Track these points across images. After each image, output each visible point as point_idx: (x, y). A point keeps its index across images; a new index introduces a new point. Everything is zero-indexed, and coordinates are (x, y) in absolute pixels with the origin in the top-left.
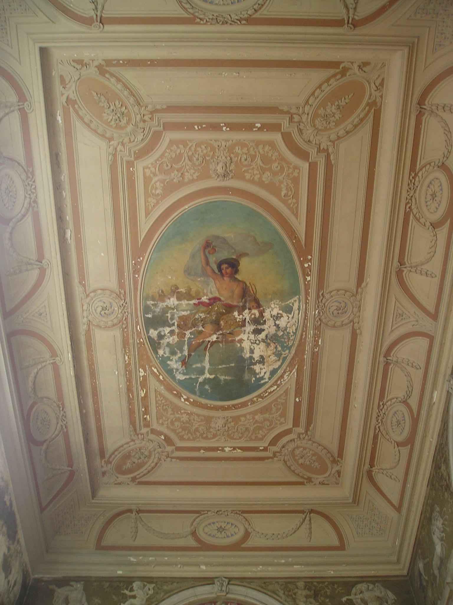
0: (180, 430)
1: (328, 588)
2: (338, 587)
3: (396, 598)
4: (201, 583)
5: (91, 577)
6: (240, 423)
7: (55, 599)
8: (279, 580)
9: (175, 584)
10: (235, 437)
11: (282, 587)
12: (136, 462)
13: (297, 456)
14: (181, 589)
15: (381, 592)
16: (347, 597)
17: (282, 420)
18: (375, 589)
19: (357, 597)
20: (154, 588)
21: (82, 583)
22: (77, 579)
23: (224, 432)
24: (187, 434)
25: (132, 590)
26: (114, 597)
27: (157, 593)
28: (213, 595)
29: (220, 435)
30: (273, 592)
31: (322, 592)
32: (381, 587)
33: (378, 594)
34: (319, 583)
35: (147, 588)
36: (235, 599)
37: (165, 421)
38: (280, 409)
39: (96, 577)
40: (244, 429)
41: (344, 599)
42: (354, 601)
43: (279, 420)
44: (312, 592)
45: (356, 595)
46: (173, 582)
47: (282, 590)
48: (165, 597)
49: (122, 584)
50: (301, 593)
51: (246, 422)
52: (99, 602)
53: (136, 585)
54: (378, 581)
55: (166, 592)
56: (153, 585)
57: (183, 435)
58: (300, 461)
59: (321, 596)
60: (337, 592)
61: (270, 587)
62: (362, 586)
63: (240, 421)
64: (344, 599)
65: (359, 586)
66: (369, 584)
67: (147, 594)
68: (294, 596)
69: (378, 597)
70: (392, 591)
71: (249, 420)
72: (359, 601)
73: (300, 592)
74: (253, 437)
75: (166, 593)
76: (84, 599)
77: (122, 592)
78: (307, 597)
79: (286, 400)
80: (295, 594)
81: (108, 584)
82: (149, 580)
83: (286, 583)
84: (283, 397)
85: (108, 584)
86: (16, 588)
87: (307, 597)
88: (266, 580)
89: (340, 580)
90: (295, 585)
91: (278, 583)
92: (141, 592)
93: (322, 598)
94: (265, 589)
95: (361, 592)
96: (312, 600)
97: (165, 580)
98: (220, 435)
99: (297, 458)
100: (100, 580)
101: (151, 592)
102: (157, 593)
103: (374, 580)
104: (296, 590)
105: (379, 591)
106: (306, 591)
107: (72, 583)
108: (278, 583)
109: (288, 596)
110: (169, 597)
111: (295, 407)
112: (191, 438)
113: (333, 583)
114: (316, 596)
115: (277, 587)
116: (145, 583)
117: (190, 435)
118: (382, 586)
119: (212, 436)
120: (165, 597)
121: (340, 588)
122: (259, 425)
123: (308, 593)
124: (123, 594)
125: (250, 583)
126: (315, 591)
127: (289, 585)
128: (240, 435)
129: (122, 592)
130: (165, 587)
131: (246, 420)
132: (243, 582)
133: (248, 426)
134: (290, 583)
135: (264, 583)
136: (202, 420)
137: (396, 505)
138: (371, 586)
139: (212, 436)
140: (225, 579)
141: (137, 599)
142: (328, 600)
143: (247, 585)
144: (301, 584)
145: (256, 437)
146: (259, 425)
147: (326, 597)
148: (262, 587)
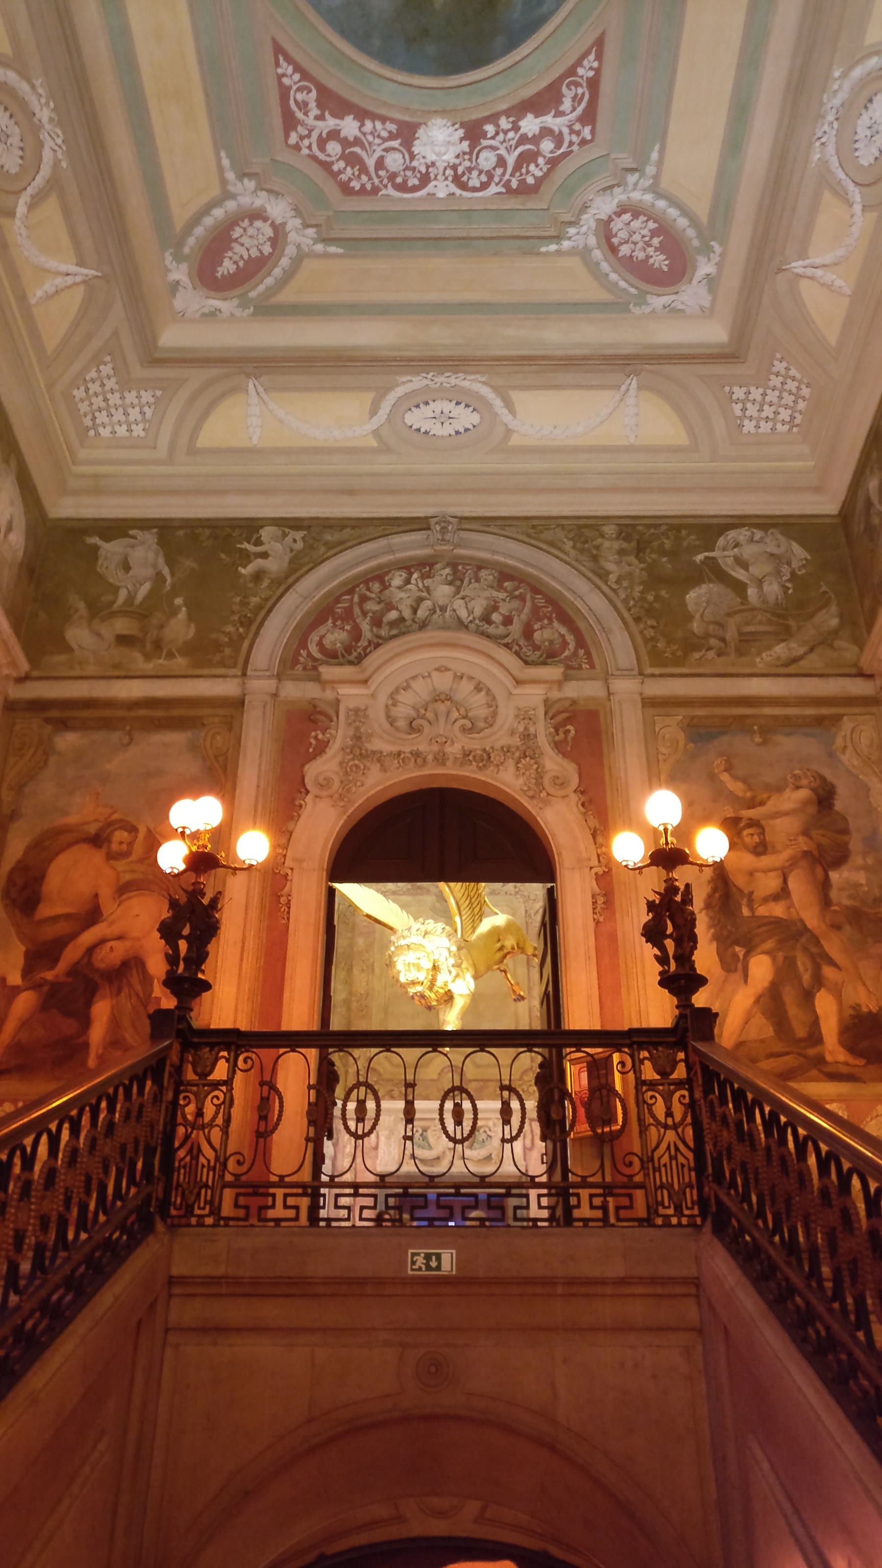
0: (342, 164)
1: (668, 538)
2: (689, 535)
3: (809, 557)
4: (400, 529)
5: (172, 520)
6: (485, 143)
7: (100, 562)
8: (565, 522)
9: (348, 529)
10: (471, 184)
11: (571, 535)
12: (246, 257)
13: (616, 235)
14: (360, 540)
15: (779, 547)
16: (706, 554)
17: (587, 132)
18: (767, 540)
19: (726, 553)
20: (303, 538)
21: (155, 530)
22: (145, 524)
23: (445, 169)
24: (359, 177)
25: (258, 542)
26: (223, 556)
27: (311, 547)
28: (428, 551)
29: (436, 179)
30: (552, 544)
31: (655, 544)
32: (780, 537)
33: (771, 548)
34: (650, 526)
35: (289, 539)
36: (471, 558)
37: (302, 138)
38: (583, 94)
39: (183, 520)
40: (493, 160)
41: (699, 558)
42: (720, 561)
43: (578, 133)
44: (634, 544)
45: (724, 549)
46: (343, 527)
47: (571, 539)
48: (329, 554)
49: (236, 533)
50: (610, 546)
51: (501, 137)
52: (194, 565)
53: (266, 533)
54: (774, 526)
55: (330, 546)
56: (302, 533)
57: (350, 180)
58: (625, 250)
59: (652, 551)
60: (685, 543)
61: (548, 535)
62: (741, 535)
63: (484, 135)
64: (699, 558)
65: (732, 534)
66: (755, 531)
67: (292, 551)
68: (595, 552)
69: (772, 555)
70: (802, 545)
71: (506, 132)
72: (730, 561)
73: (607, 544)
74: (514, 184)
75: (329, 549)
76: (161, 560)
77: (239, 546)
78: (621, 552)
79: (598, 71)
80: (597, 547)
81: (207, 532)
82: (295, 524)
83: (580, 527)
84: (591, 61)
85: (207, 532)
86: (12, 537)
87: (621, 552)
88: (535, 522)
89: (691, 521)
90: (598, 530)
91: (563, 527)
92: (278, 546)
93: (654, 556)
94: (537, 540)
95: (737, 545)
96: (632, 559)
97: (328, 524)
98: (436, 179)
99: (615, 241)
100: (192, 526)
101: (300, 545)
102: (311, 547)
103: (766, 523)
104: (600, 540)
105: (776, 543)
106: (621, 542)
107: (131, 532)
108: (563, 527)
109: (582, 551)
110: (335, 555)
111: (674, 71)
112: (369, 187)
113: (678, 528)
114: (639, 551)
115: (561, 534)
116: (287, 530)
117: (364, 178)
118: (782, 533)
119: (417, 182)
120: (329, 554)
121: (693, 537)
122: (528, 147)
123: (625, 545)
124: (241, 549)
125: (503, 527)
126: (638, 542)
127: (583, 530)
128: (484, 178)
129: (239, 546)
130: (328, 537)
131: (497, 133)
132: (489, 526)
133: (502, 151)
134: (586, 526)
135: (534, 527)
136: (392, 137)
137: (771, 822)
138: (758, 534)
139: (417, 182)
140: (451, 520)
141: (270, 558)
142: (664, 559)
143: (496, 531)
144: (610, 530)
145: (522, 182)
146: (528, 147)
147: (663, 552)
148: (529, 536)
